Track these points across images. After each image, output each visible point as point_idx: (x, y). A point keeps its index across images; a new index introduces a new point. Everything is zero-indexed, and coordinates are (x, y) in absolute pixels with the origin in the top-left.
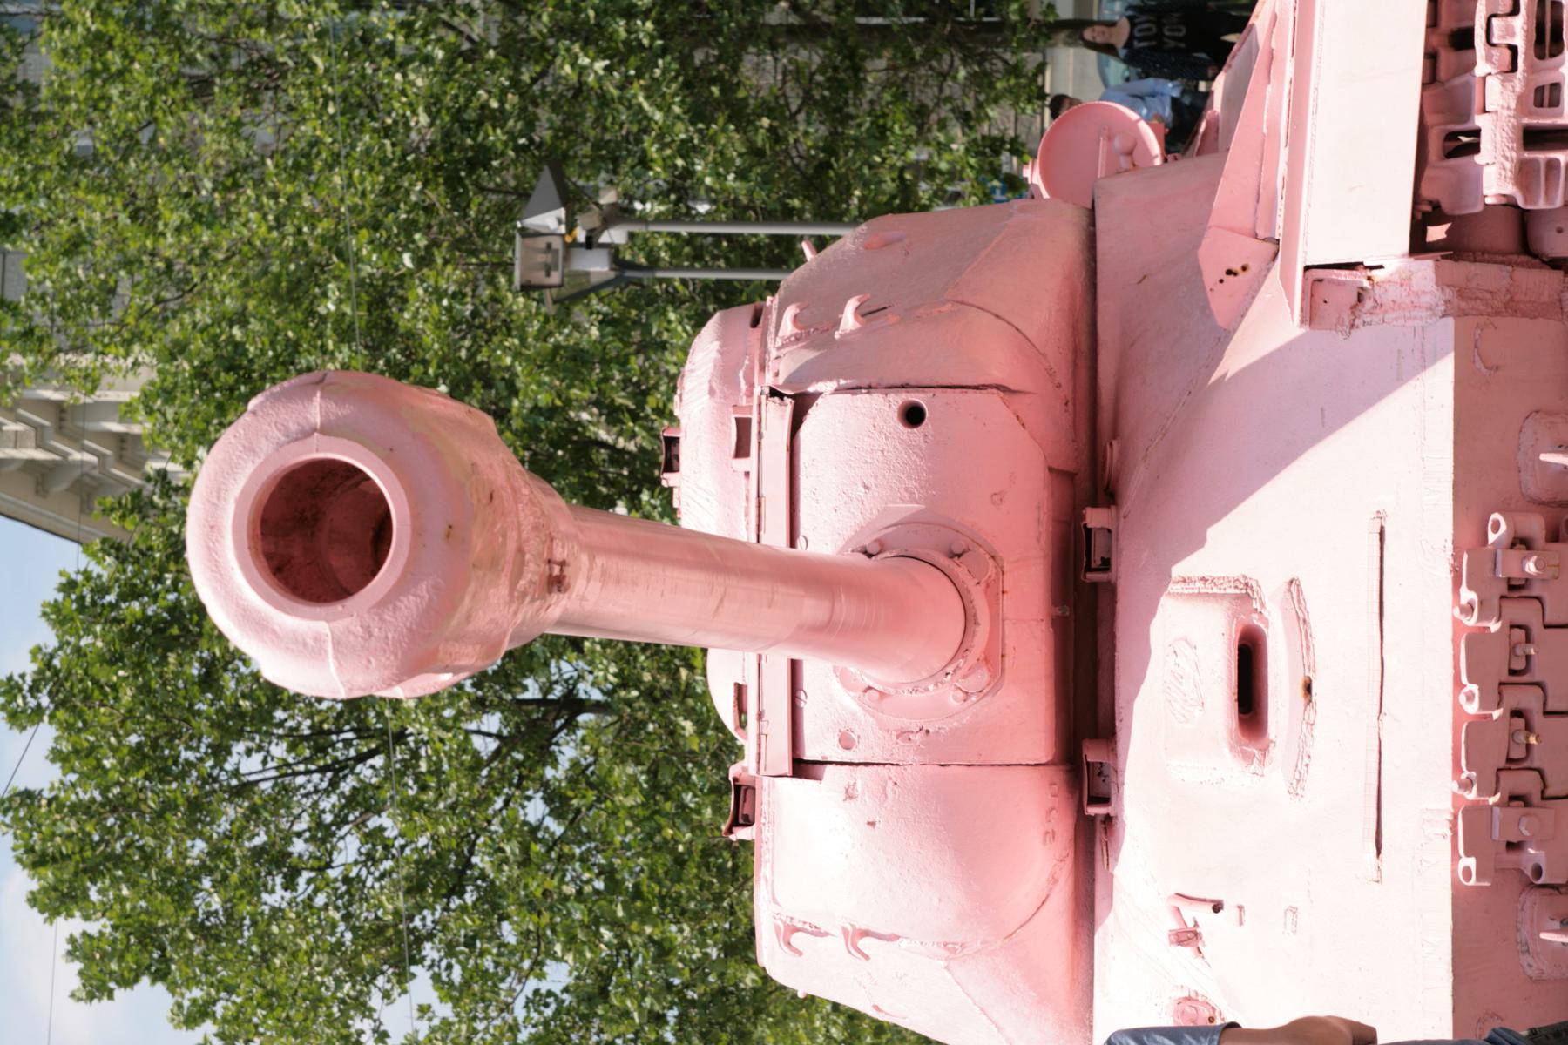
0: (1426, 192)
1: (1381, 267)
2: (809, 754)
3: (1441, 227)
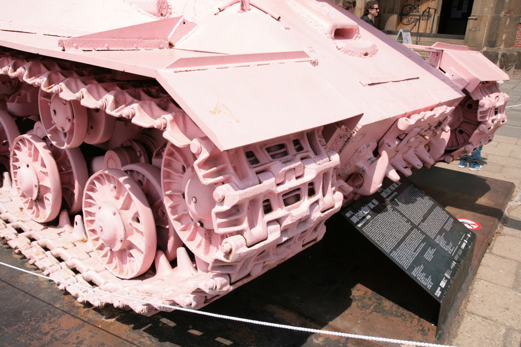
1: (445, 73)
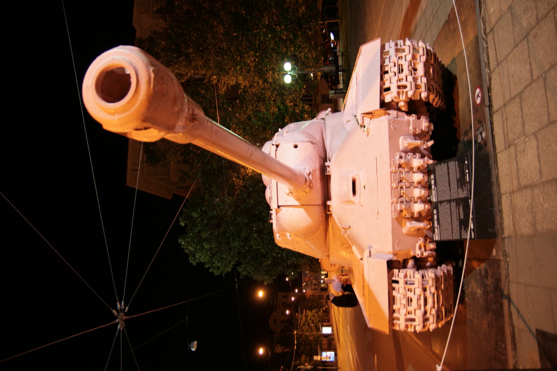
0: (382, 98)
2: (279, 205)
3: (384, 105)
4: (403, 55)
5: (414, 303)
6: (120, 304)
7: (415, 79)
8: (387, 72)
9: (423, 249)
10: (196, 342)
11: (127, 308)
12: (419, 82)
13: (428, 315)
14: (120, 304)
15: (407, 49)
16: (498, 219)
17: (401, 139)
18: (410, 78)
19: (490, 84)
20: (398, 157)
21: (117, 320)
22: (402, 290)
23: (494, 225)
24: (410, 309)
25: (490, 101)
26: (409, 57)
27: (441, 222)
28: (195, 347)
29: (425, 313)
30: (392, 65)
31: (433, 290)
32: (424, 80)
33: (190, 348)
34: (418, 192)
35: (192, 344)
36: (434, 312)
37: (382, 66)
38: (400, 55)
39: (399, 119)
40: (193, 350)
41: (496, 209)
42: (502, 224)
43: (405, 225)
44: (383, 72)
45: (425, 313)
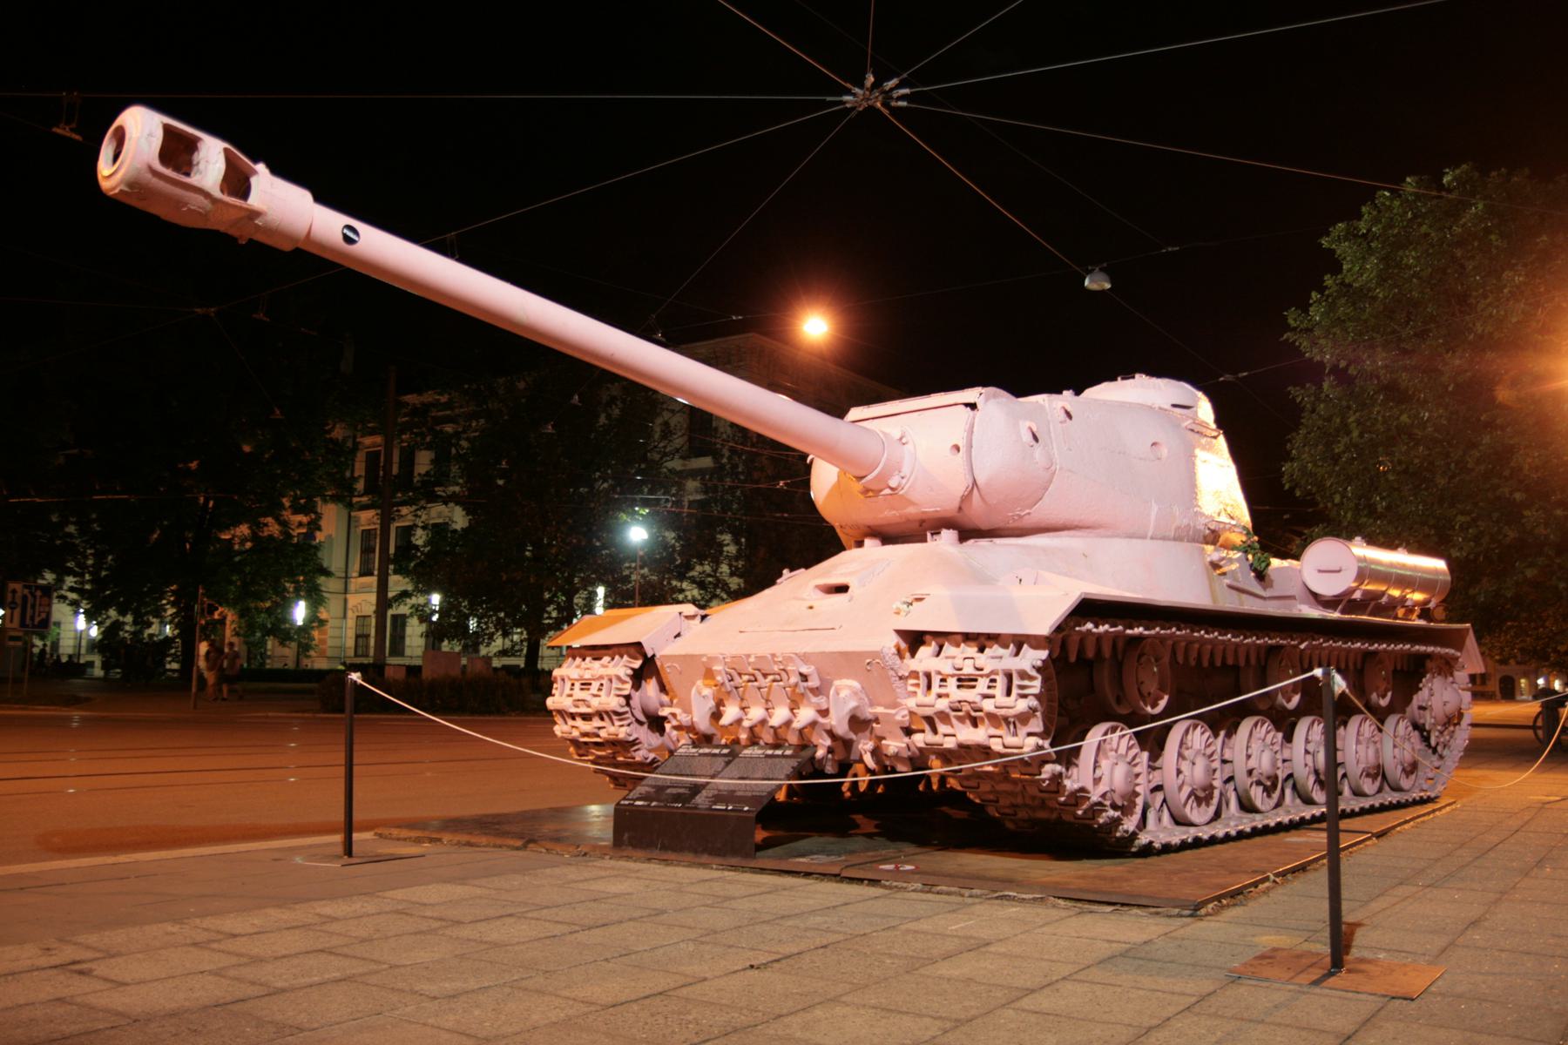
0: (928, 638)
3: (914, 640)
4: (999, 690)
5: (578, 694)
6: (898, 87)
7: (944, 717)
8: (981, 650)
9: (675, 723)
10: (1108, 286)
11: (901, 103)
12: (942, 728)
13: (571, 722)
14: (898, 87)
15: (931, 698)
16: (640, 853)
17: (855, 684)
18: (942, 705)
19: (885, 887)
20: (804, 670)
21: (857, 90)
22: (603, 671)
23: (635, 847)
24: (577, 685)
25: (852, 880)
26: (988, 705)
27: (706, 759)
28: (1095, 287)
29: (573, 716)
30: (979, 664)
31: (603, 733)
32: (950, 743)
33: (1089, 272)
34: (756, 713)
35: (1102, 276)
36: (576, 733)
37: (994, 638)
38: (1001, 682)
39: (899, 683)
40: (1087, 283)
41: (656, 853)
42: (628, 858)
43: (707, 686)
44: (982, 641)
45: (573, 716)
